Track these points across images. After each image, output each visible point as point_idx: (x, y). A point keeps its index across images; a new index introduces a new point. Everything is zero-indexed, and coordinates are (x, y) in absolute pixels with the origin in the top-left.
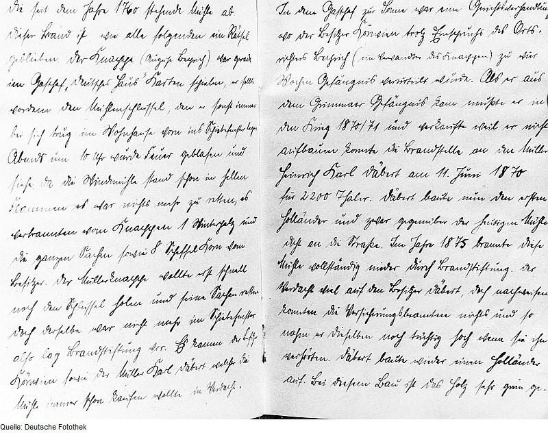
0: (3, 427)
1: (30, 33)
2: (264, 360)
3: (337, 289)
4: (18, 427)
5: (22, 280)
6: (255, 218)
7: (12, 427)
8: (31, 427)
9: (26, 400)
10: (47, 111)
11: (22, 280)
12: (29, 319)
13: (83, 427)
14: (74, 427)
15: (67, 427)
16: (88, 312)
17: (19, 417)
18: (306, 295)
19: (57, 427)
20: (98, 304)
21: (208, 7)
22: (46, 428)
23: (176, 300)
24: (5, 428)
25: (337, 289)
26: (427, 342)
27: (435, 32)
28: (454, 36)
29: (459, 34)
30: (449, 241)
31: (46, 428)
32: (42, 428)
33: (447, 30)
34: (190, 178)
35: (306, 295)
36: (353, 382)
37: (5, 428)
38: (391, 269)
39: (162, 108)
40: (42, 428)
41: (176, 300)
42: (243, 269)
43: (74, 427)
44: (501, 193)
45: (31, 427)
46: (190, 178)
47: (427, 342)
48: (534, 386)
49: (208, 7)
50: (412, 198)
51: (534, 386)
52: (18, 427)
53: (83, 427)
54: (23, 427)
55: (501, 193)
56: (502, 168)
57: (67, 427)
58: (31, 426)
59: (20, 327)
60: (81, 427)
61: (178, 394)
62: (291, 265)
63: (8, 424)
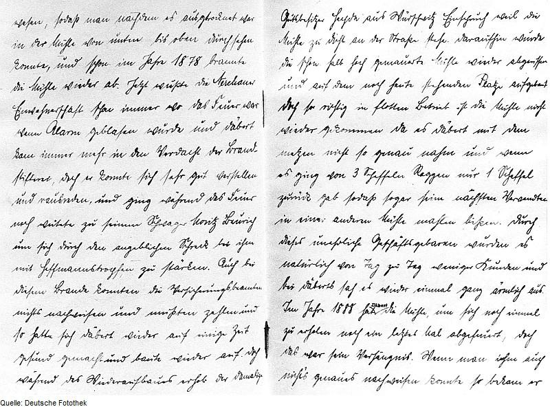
0: (3, 403)
3: (297, 105)
4: (18, 403)
7: (12, 402)
8: (31, 403)
13: (83, 403)
14: (75, 403)
15: (67, 403)
17: (22, 393)
22: (46, 404)
25: (297, 105)
27: (446, 18)
28: (464, 21)
29: (469, 19)
31: (46, 404)
32: (42, 404)
33: (457, 15)
34: (99, 63)
37: (5, 404)
39: (537, 314)
40: (42, 404)
43: (75, 403)
44: (402, 287)
45: (31, 403)
46: (99, 63)
47: (130, 204)
50: (465, 130)
52: (18, 403)
53: (83, 403)
54: (23, 403)
55: (402, 287)
57: (67, 403)
58: (32, 402)
60: (81, 403)
61: (515, 107)
62: (393, 220)
63: (8, 400)
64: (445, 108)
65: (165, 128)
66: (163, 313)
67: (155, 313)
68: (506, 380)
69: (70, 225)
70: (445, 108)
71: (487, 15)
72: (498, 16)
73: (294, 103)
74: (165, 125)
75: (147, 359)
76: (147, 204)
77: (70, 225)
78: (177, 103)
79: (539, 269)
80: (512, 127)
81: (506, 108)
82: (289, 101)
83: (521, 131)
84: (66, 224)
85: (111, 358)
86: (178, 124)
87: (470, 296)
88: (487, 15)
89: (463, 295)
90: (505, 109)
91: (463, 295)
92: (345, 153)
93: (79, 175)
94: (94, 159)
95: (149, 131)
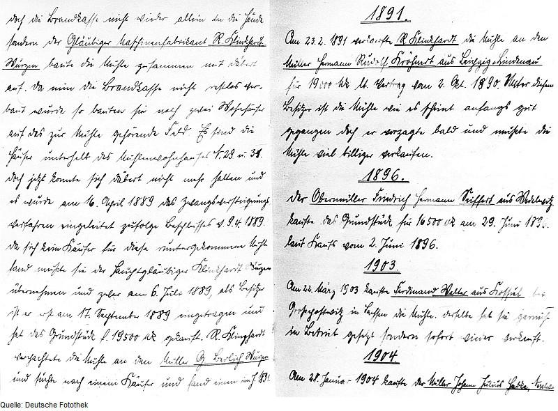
0: (3, 405)
4: (18, 405)
6: (90, 289)
7: (12, 404)
8: (32, 405)
12: (510, 284)
13: (84, 405)
14: (76, 405)
15: (68, 405)
19: (58, 405)
20: (206, 224)
21: (102, 357)
22: (47, 405)
24: (5, 406)
30: (377, 174)
31: (47, 405)
32: (43, 406)
37: (5, 406)
40: (43, 406)
42: (14, 225)
43: (76, 405)
45: (32, 405)
48: (522, 106)
49: (102, 357)
51: (522, 106)
52: (18, 405)
53: (84, 405)
54: (24, 405)
56: (251, 218)
57: (68, 405)
58: (32, 404)
59: (298, 191)
60: (82, 404)
63: (8, 401)
64: (451, 109)
65: (39, 200)
66: (505, 133)
68: (389, 379)
70: (451, 109)
71: (104, 176)
73: (352, 128)
74: (39, 197)
75: (406, 154)
79: (481, 132)
80: (11, 176)
82: (347, 128)
85: (253, 12)
88: (104, 176)
93: (357, 128)
94: (547, 84)
95: (25, 203)
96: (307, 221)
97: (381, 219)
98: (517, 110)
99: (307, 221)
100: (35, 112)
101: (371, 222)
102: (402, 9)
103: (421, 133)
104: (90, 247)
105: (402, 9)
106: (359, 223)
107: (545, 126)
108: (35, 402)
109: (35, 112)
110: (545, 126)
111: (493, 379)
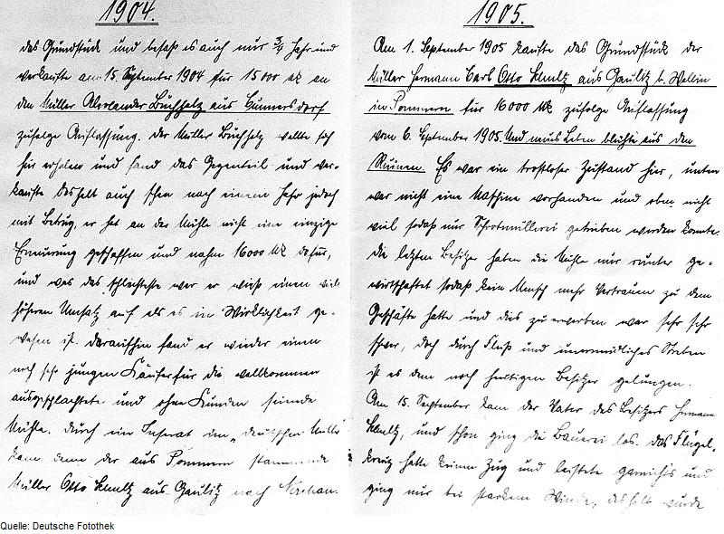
0: (4, 526)
1: (564, 167)
2: (373, 228)
4: (23, 527)
5: (570, 375)
7: (15, 525)
8: (41, 526)
9: (21, 423)
10: (672, 231)
11: (632, 407)
12: (503, 166)
13: (109, 526)
14: (98, 526)
15: (88, 526)
16: (104, 143)
18: (128, 85)
19: (76, 526)
22: (61, 527)
23: (637, 173)
24: (6, 527)
26: (418, 202)
31: (61, 527)
32: (56, 527)
35: (128, 85)
36: (273, 400)
37: (6, 527)
38: (530, 408)
40: (56, 527)
41: (637, 173)
43: (98, 526)
45: (41, 526)
47: (418, 202)
52: (23, 527)
53: (109, 526)
54: (31, 527)
57: (88, 526)
58: (42, 525)
60: (107, 525)
63: (11, 522)
67: (286, 374)
69: (549, 50)
72: (534, 199)
75: (269, 372)
76: (132, 140)
77: (549, 50)
78: (467, 165)
81: (195, 223)
83: (120, 197)
84: (92, 401)
86: (97, 334)
87: (500, 444)
89: (308, 204)
90: (193, 225)
91: (308, 204)
92: (242, 224)
96: (37, 192)
97: (652, 46)
98: (315, 316)
99: (37, 192)
100: (174, 286)
101: (640, 51)
102: (411, 44)
103: (413, 317)
104: (114, 221)
105: (411, 44)
106: (292, 167)
107: (215, 366)
108: (46, 522)
109: (174, 286)
110: (215, 366)
111: (484, 190)
